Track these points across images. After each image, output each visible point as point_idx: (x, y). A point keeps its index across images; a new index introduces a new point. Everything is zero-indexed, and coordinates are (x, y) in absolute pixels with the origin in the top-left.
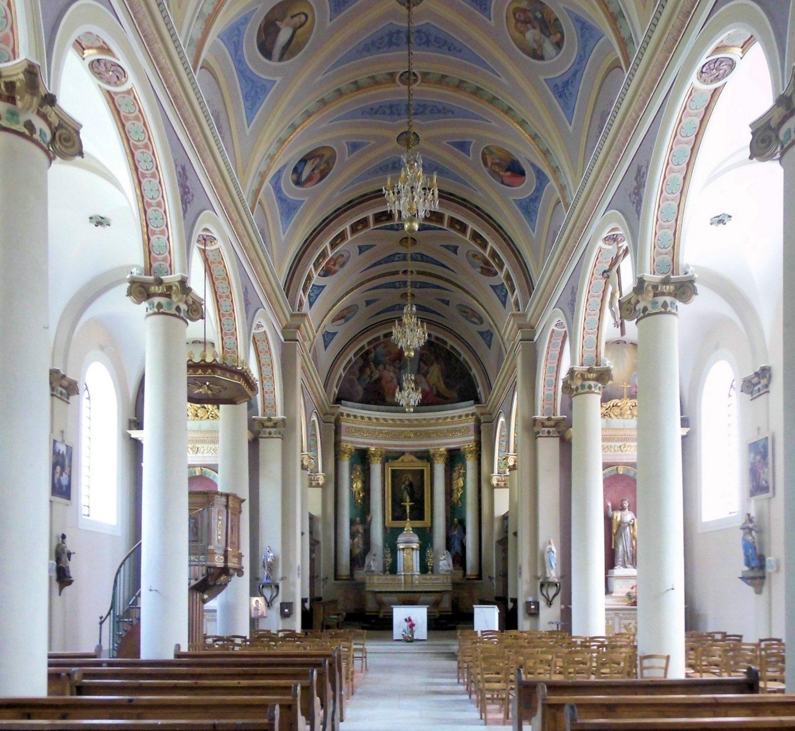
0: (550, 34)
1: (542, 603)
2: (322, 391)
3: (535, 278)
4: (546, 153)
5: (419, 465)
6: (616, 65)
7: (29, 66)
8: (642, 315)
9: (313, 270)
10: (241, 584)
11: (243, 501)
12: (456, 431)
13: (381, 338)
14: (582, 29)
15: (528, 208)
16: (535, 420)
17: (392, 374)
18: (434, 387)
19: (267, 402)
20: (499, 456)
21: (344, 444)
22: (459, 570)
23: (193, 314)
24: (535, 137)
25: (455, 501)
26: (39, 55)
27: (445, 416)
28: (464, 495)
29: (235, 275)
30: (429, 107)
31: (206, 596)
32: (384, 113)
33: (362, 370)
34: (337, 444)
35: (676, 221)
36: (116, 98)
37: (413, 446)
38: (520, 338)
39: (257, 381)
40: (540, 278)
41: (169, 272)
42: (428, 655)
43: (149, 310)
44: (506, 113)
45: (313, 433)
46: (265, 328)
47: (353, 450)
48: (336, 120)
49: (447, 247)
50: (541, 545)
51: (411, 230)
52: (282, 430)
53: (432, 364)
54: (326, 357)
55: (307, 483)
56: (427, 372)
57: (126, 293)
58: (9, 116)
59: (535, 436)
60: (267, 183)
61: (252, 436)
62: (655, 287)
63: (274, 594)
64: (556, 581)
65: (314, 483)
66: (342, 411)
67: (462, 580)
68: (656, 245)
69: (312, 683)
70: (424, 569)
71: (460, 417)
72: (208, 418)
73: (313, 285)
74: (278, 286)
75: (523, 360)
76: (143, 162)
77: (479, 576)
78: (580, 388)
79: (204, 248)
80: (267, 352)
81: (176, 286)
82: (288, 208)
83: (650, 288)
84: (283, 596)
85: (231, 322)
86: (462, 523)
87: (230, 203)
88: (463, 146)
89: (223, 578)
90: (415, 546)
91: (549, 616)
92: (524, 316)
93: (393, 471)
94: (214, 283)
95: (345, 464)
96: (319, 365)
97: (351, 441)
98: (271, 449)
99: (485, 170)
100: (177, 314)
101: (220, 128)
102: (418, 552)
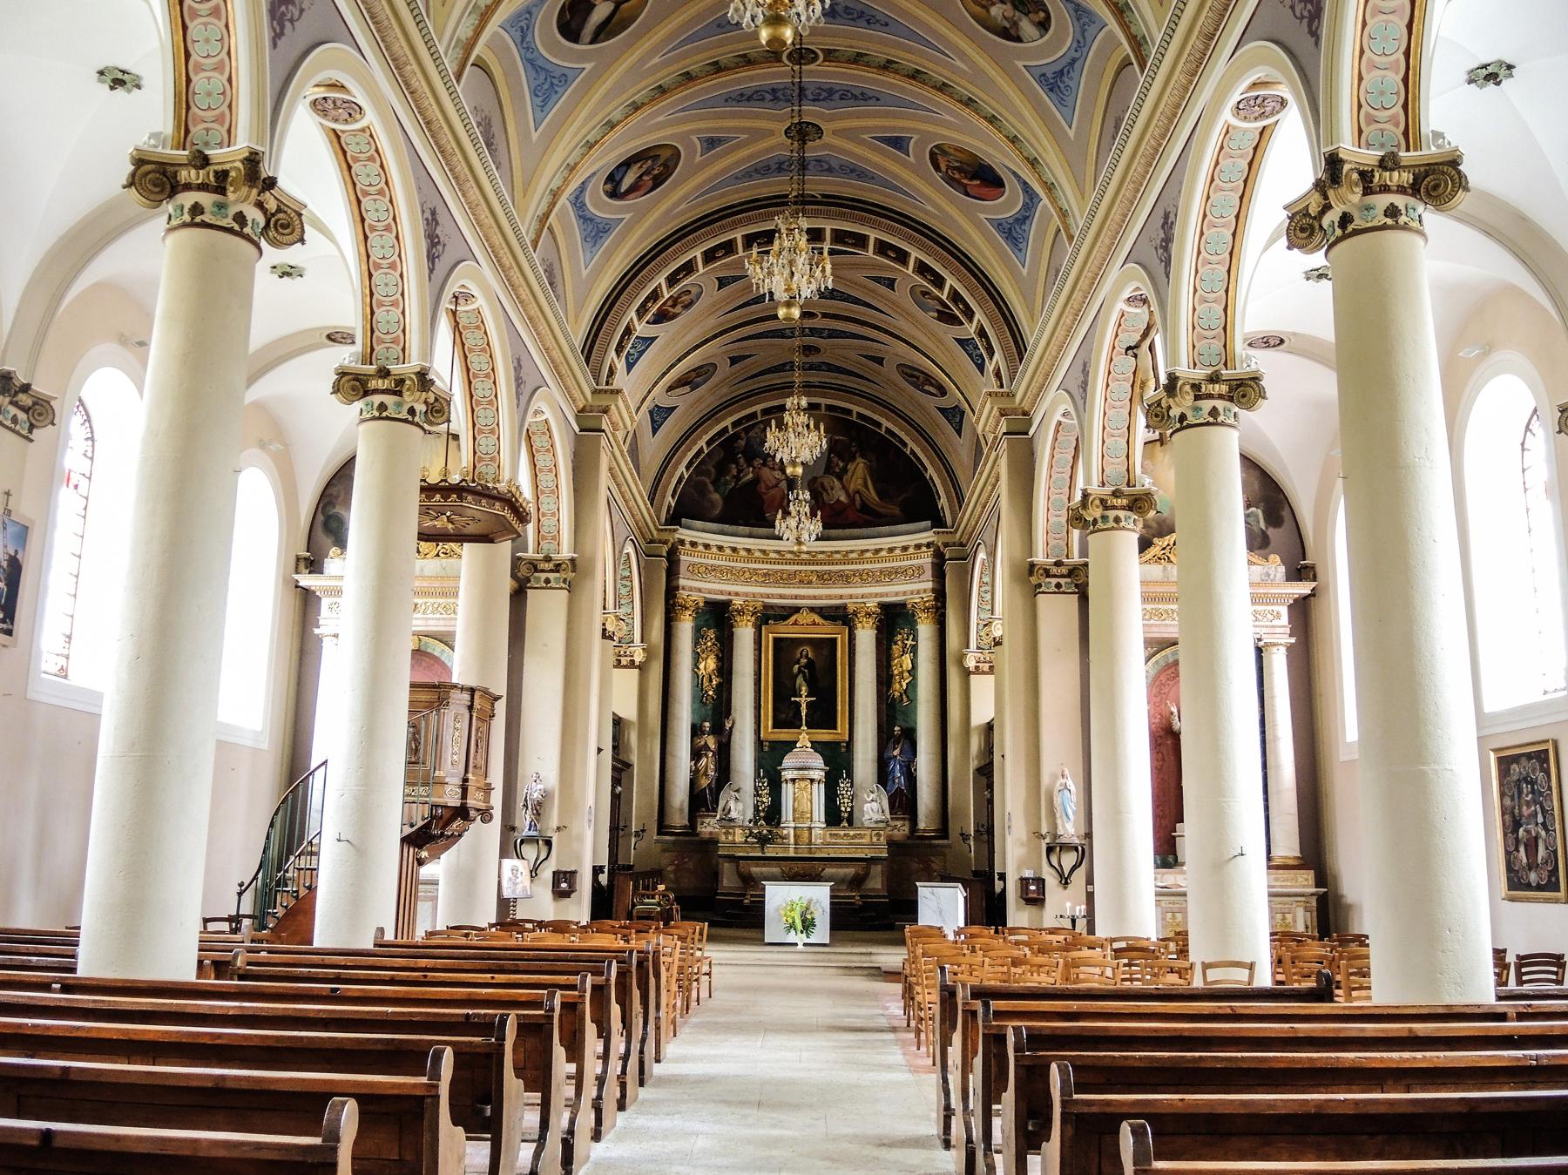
0: (1029, 12)
1: (1051, 881)
2: (645, 504)
3: (1028, 333)
4: (1033, 163)
5: (825, 630)
6: (1126, 63)
7: (251, 153)
8: (1178, 425)
9: (635, 320)
10: (486, 835)
11: (498, 698)
12: (896, 572)
13: (759, 414)
14: (1076, 11)
15: (1013, 232)
16: (1032, 565)
18: (857, 497)
19: (544, 530)
20: (978, 618)
21: (683, 594)
22: (903, 819)
23: (433, 416)
24: (1014, 140)
25: (897, 694)
26: (261, 141)
27: (878, 547)
28: (913, 685)
29: (502, 346)
30: (837, 91)
31: (424, 854)
32: (763, 99)
33: (722, 469)
34: (671, 591)
35: (1227, 291)
36: (343, 137)
37: (815, 598)
38: (1004, 430)
39: (528, 503)
40: (1036, 336)
41: (401, 361)
42: (830, 970)
43: (364, 413)
44: (967, 105)
45: (627, 574)
46: (548, 415)
47: (701, 604)
48: (683, 110)
49: (877, 280)
50: (1045, 779)
51: (788, 319)
52: (571, 575)
53: (853, 459)
54: (654, 448)
55: (613, 660)
56: (845, 470)
57: (331, 390)
58: (216, 209)
59: (1036, 590)
60: (563, 200)
61: (516, 585)
62: (1196, 387)
63: (543, 856)
64: (1077, 841)
65: (624, 661)
66: (682, 537)
67: (908, 838)
68: (1196, 325)
69: (608, 980)
70: (834, 816)
71: (905, 549)
72: (438, 555)
73: (637, 337)
74: (573, 350)
75: (1010, 466)
76: (387, 246)
77: (943, 831)
78: (1100, 520)
79: (453, 308)
80: (548, 450)
81: (411, 379)
82: (596, 231)
83: (1187, 388)
84: (558, 861)
85: (490, 413)
86: (910, 736)
87: (500, 244)
88: (898, 143)
89: (457, 824)
90: (818, 775)
91: (1062, 904)
92: (1011, 395)
94: (466, 357)
95: (685, 627)
96: (641, 463)
97: (696, 588)
98: (547, 607)
99: (937, 176)
100: (410, 418)
101: (489, 145)
102: (822, 786)
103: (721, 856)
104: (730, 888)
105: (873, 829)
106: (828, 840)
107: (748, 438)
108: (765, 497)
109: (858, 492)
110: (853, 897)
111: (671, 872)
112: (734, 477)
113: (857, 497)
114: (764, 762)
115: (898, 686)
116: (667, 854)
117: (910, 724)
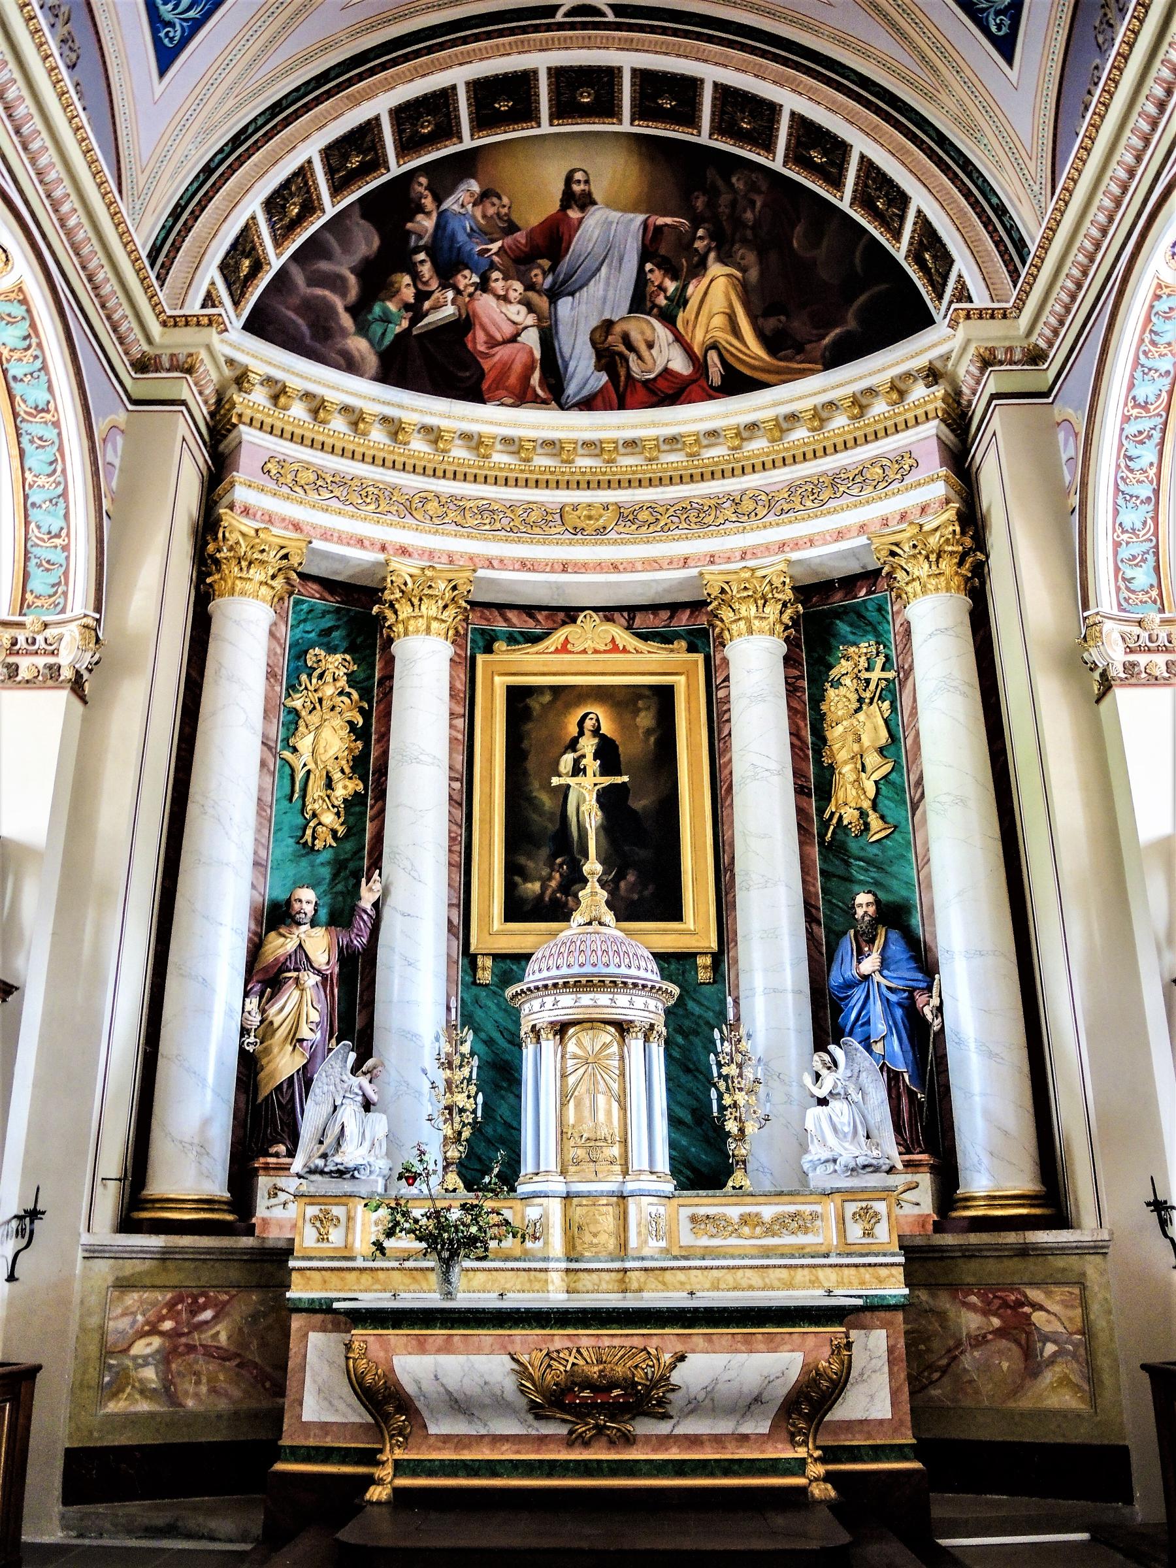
17: (517, 313)
18: (713, 356)
25: (850, 815)
53: (699, 268)
56: (680, 300)
93: (518, 697)
102: (658, 1052)
103: (298, 1308)
104: (324, 1427)
105: (849, 1194)
106: (686, 1238)
107: (441, 215)
108: (486, 365)
109: (714, 346)
110: (799, 1466)
111: (145, 1361)
112: (407, 307)
113: (713, 356)
114: (479, 1014)
115: (852, 792)
116: (132, 1299)
117: (899, 892)
